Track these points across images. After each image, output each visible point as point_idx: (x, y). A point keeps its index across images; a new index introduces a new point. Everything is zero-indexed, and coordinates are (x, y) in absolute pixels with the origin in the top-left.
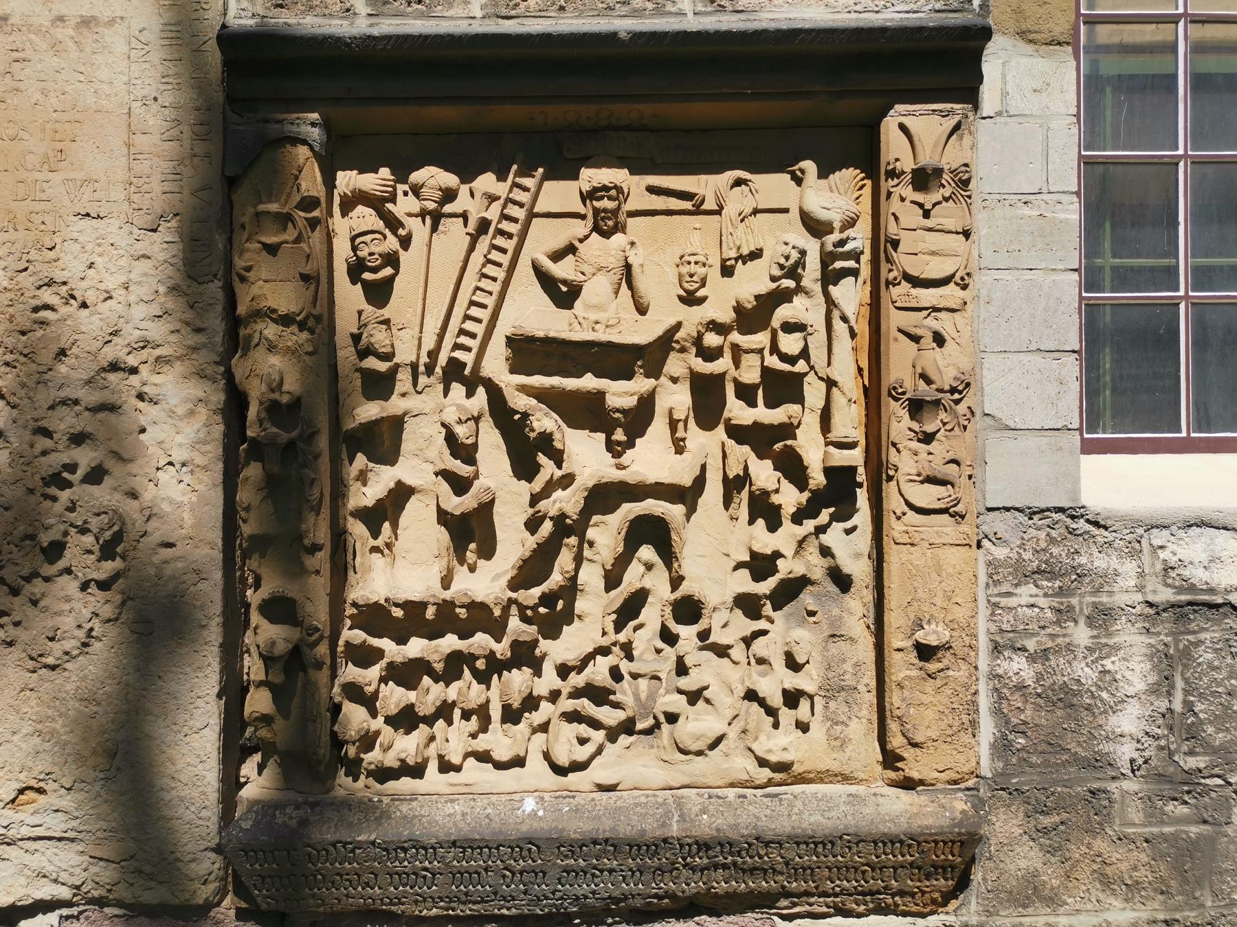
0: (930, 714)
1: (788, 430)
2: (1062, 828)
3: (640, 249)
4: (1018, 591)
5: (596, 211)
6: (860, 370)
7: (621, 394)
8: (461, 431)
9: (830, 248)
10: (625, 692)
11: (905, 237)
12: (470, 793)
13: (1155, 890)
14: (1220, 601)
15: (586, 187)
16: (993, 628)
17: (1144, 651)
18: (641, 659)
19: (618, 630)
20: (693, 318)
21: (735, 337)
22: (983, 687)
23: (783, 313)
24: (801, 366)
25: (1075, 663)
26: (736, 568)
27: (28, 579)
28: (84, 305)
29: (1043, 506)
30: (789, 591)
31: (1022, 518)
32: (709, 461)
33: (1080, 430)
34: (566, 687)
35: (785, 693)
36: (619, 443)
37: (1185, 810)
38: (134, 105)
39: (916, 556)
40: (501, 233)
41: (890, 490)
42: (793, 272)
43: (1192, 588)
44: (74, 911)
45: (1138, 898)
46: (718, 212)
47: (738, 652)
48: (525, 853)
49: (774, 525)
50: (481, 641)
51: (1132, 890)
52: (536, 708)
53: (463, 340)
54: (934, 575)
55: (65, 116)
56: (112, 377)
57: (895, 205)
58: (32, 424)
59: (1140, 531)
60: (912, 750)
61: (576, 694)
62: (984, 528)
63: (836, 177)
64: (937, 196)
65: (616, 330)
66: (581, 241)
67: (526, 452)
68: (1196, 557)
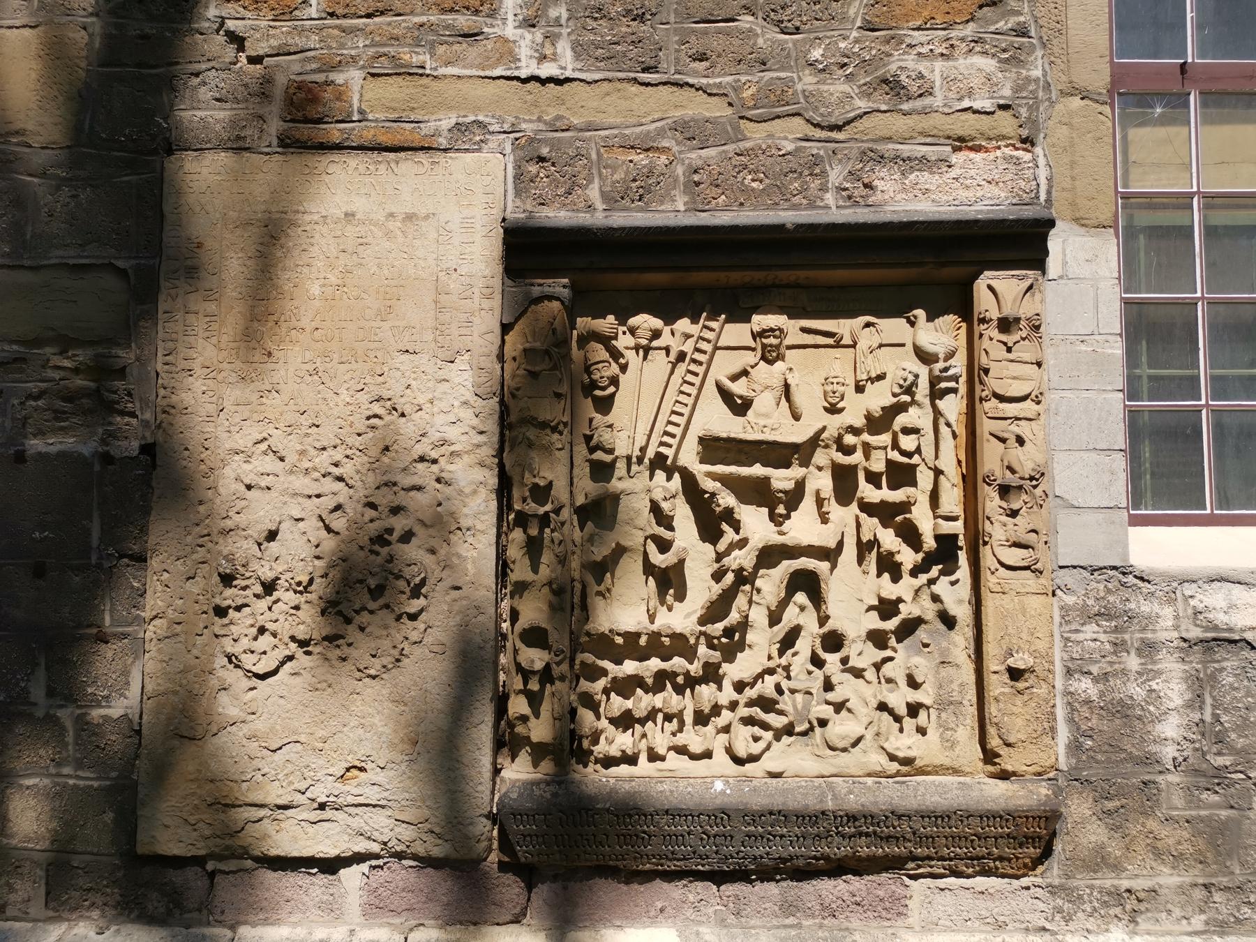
0: (1020, 722)
1: (905, 507)
2: (1122, 810)
3: (796, 374)
4: (1084, 628)
5: (764, 346)
6: (959, 462)
7: (782, 479)
8: (665, 506)
9: (937, 373)
10: (786, 703)
11: (993, 367)
12: (673, 776)
13: (1195, 860)
14: (1237, 638)
15: (756, 329)
16: (1066, 657)
17: (1181, 675)
18: (796, 679)
19: (780, 656)
20: (834, 424)
21: (866, 437)
22: (1059, 702)
23: (901, 420)
24: (916, 459)
25: (1128, 684)
26: (867, 611)
27: (357, 612)
28: (403, 415)
29: (1101, 565)
30: (909, 628)
31: (1086, 574)
32: (846, 529)
33: (1127, 508)
34: (743, 699)
36: (781, 516)
37: (1216, 798)
38: (441, 274)
39: (1007, 602)
40: (694, 361)
41: (986, 552)
42: (909, 390)
43: (1216, 628)
44: (380, 862)
45: (1182, 866)
46: (854, 346)
47: (870, 674)
48: (719, 820)
49: (896, 578)
50: (678, 663)
51: (1178, 858)
52: (719, 715)
53: (666, 439)
54: (1020, 616)
55: (392, 283)
56: (420, 466)
57: (986, 343)
58: (364, 500)
59: (1175, 584)
60: (1006, 749)
61: (751, 703)
62: (1058, 581)
63: (940, 321)
64: (1016, 337)
65: (777, 433)
66: (752, 367)
67: (711, 523)
68: (1222, 606)
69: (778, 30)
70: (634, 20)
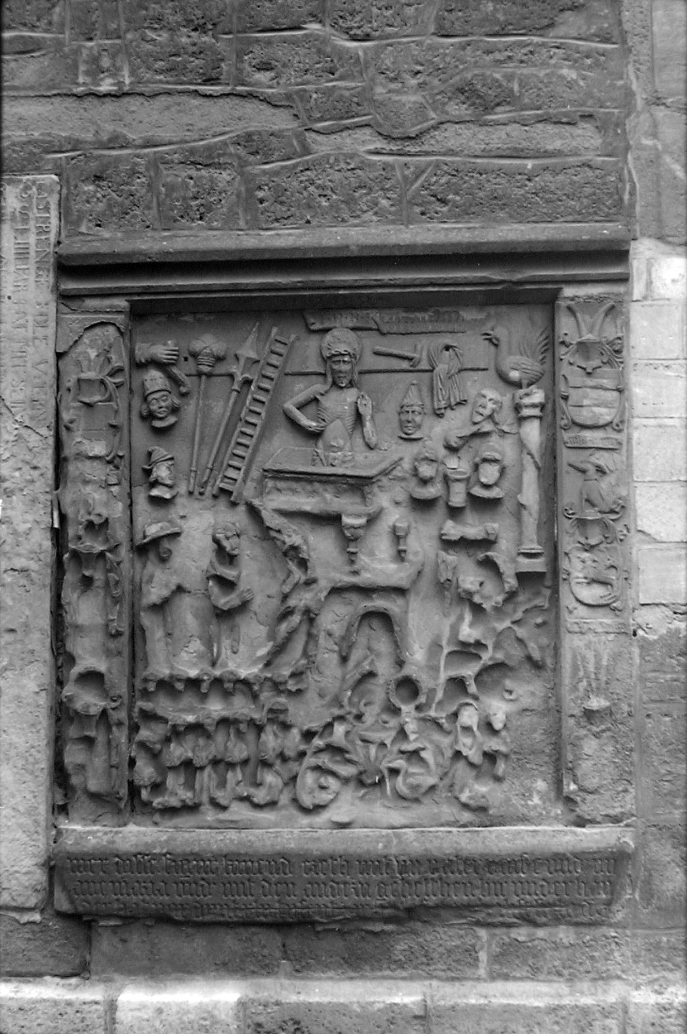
10: (358, 753)
35: (486, 754)
46: (432, 371)
69: (347, 37)
70: (195, 30)
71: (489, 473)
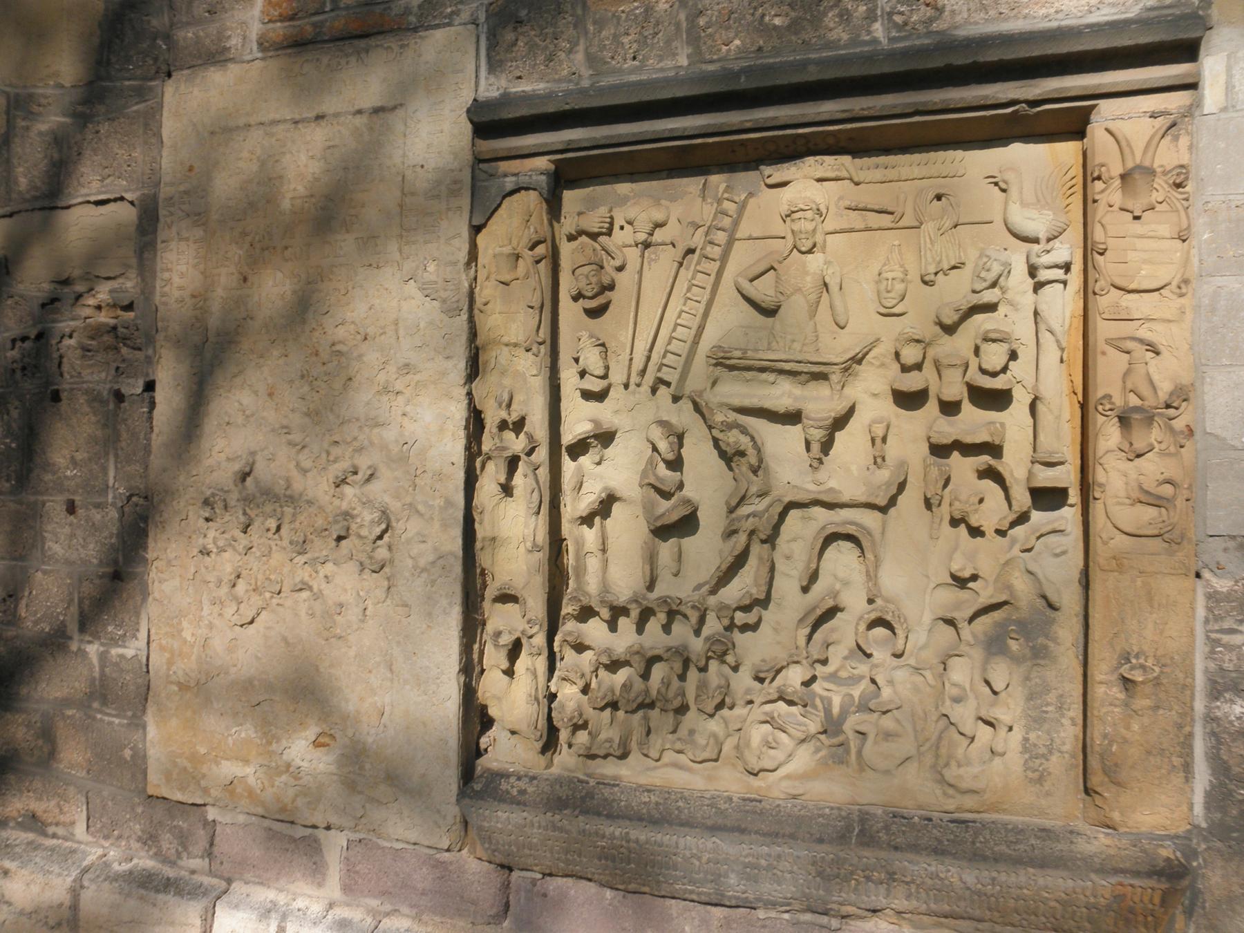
7: (819, 402)
16: (1212, 666)
71: (994, 356)
